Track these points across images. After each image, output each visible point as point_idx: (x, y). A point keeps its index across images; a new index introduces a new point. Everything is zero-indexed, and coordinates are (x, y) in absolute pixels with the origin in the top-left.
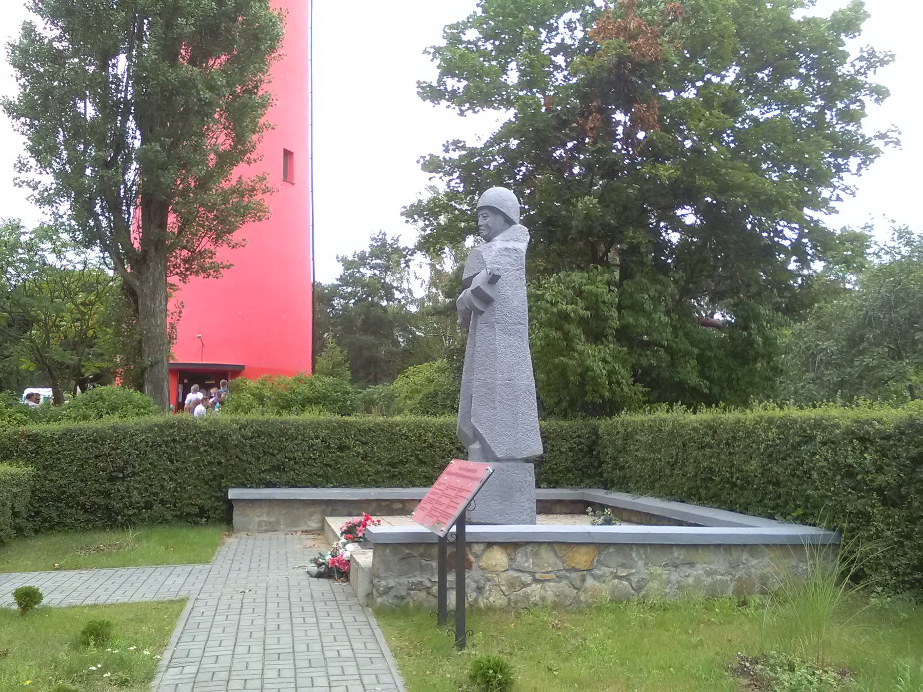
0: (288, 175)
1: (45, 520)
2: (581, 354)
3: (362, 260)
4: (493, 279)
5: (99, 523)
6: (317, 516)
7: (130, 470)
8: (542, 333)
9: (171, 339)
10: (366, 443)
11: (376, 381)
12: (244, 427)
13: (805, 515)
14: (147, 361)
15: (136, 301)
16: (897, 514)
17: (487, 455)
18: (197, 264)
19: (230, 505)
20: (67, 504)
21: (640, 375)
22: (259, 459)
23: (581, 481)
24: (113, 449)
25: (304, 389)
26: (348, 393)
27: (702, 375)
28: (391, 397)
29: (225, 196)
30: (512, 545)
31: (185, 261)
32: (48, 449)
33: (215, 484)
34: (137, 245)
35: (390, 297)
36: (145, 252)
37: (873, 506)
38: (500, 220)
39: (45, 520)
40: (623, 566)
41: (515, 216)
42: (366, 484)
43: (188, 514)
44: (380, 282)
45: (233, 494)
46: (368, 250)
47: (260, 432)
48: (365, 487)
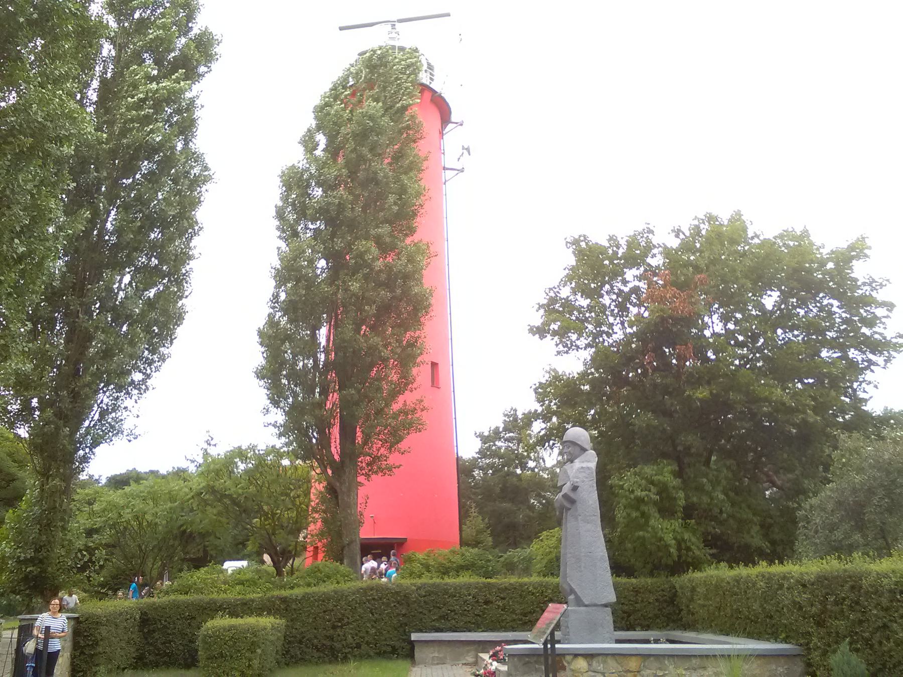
0: (435, 381)
1: (292, 657)
2: (653, 528)
3: (496, 434)
4: (575, 488)
5: (327, 659)
6: (472, 653)
7: (346, 620)
8: (625, 514)
9: (360, 523)
10: (503, 599)
11: (515, 545)
12: (419, 588)
13: (787, 637)
14: (346, 540)
15: (337, 497)
16: (822, 631)
17: (579, 602)
18: (376, 465)
19: (412, 644)
20: (306, 645)
21: (711, 541)
22: (430, 611)
23: (668, 625)
24: (336, 606)
25: (458, 559)
26: (489, 561)
27: (766, 536)
28: (529, 560)
29: (395, 416)
30: (589, 656)
31: (368, 464)
32: (294, 606)
33: (401, 630)
34: (337, 457)
35: (524, 466)
36: (342, 462)
37: (812, 627)
38: (578, 449)
39: (292, 657)
40: (660, 669)
41: (588, 444)
42: (506, 629)
43: (385, 652)
44: (513, 453)
45: (414, 636)
46: (502, 426)
47: (431, 592)
48: (505, 631)
